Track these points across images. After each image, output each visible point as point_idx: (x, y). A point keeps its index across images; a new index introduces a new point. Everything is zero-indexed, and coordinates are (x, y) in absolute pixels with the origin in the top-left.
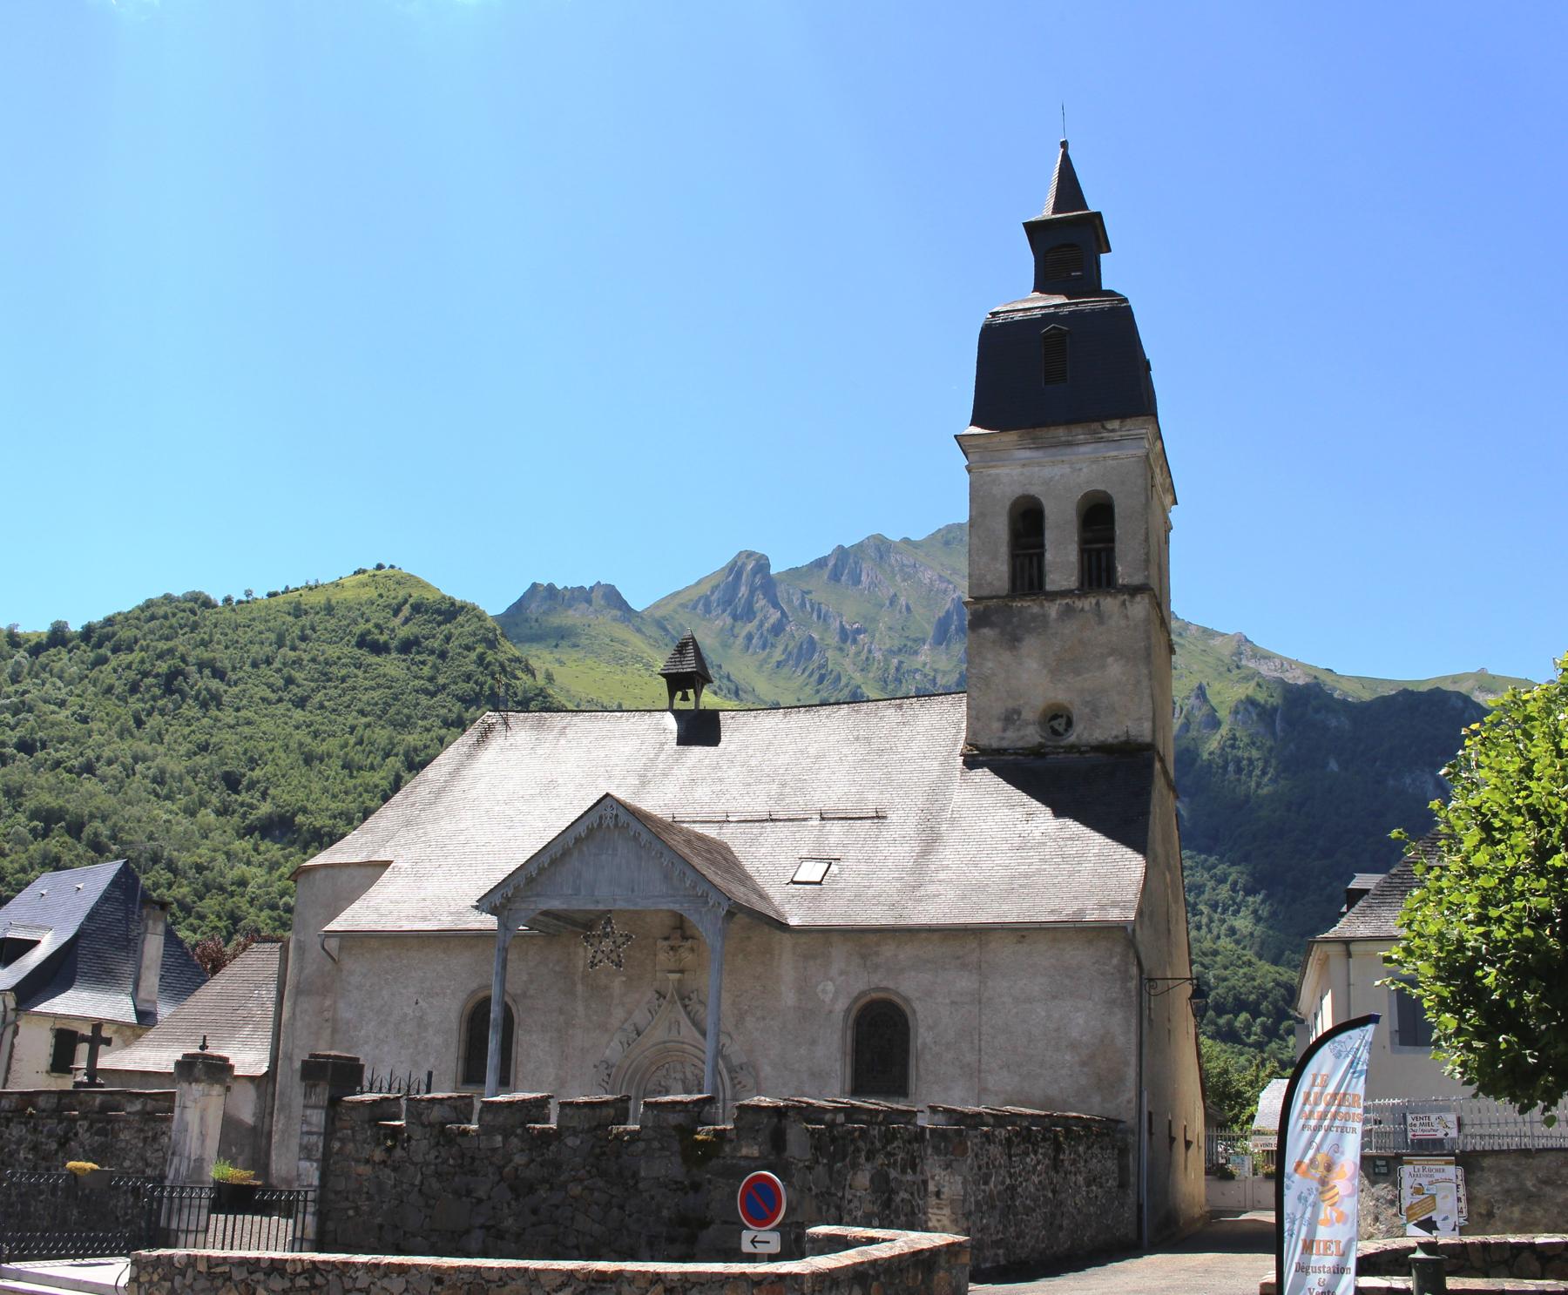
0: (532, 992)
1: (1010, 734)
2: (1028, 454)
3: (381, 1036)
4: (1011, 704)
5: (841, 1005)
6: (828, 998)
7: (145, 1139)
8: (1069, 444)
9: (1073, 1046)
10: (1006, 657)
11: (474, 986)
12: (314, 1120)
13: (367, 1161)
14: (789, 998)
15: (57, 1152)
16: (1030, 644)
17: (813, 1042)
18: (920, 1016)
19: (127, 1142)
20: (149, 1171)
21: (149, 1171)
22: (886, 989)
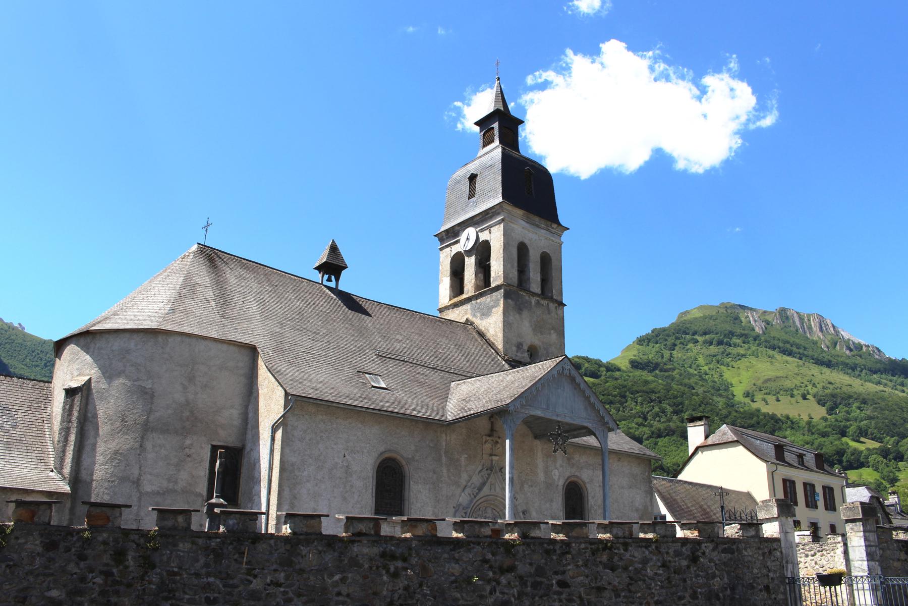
0: (417, 458)
1: (519, 354)
2: (523, 223)
3: (319, 477)
4: (519, 340)
5: (561, 483)
6: (556, 478)
7: (764, 554)
8: (538, 226)
9: (637, 510)
10: (517, 316)
11: (382, 449)
12: (871, 539)
13: (899, 560)
14: (541, 477)
15: (688, 567)
16: (525, 313)
17: (552, 501)
18: (589, 491)
19: (752, 556)
20: (771, 575)
21: (771, 575)
22: (577, 477)
